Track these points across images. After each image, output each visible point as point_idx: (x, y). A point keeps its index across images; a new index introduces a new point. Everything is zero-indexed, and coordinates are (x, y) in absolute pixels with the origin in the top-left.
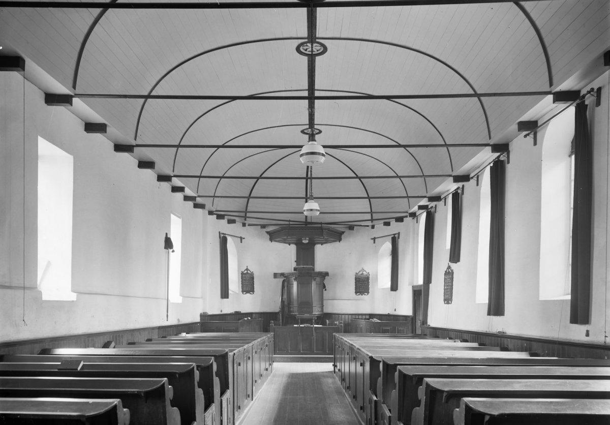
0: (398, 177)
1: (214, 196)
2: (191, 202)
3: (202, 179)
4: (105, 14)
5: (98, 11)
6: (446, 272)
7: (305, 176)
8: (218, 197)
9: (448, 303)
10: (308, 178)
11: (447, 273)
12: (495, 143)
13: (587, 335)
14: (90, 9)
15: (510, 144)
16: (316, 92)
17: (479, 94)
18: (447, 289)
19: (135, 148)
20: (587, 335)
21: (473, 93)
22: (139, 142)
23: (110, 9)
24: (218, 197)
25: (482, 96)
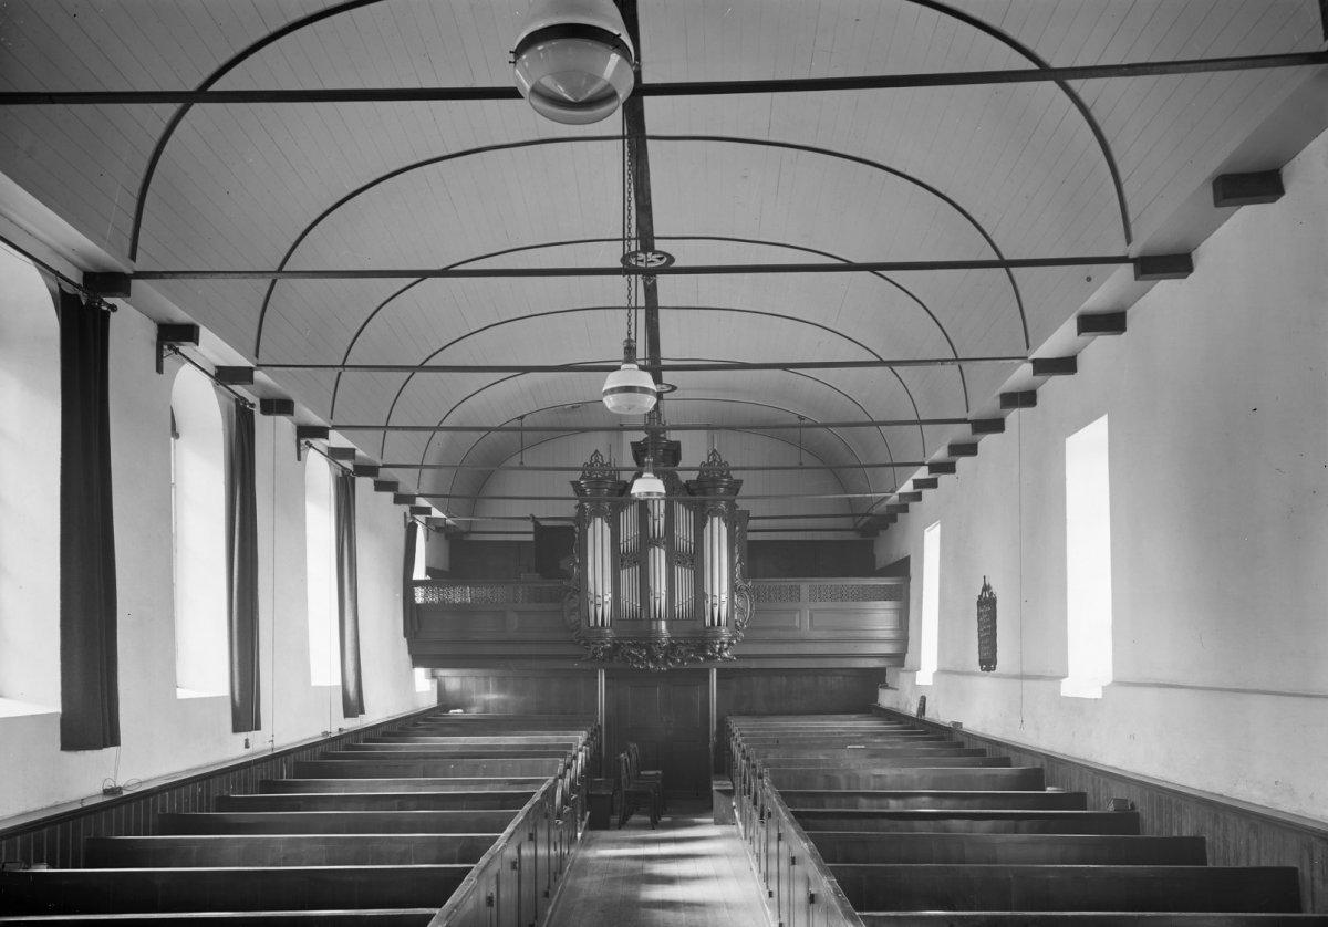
0: (1061, 76)
1: (387, 427)
2: (368, 479)
3: (391, 434)
4: (187, 115)
5: (171, 109)
6: (980, 597)
7: (621, 237)
8: (397, 428)
9: (989, 670)
10: (636, 308)
11: (982, 602)
12: (1228, 171)
13: (247, 746)
14: (156, 106)
15: (1286, 171)
16: (656, 241)
17: (1007, 261)
18: (984, 638)
19: (136, 284)
20: (247, 746)
21: (996, 258)
22: (139, 266)
23: (196, 105)
24: (397, 428)
25: (1013, 266)
